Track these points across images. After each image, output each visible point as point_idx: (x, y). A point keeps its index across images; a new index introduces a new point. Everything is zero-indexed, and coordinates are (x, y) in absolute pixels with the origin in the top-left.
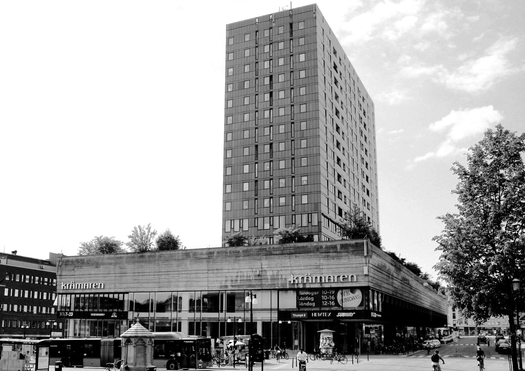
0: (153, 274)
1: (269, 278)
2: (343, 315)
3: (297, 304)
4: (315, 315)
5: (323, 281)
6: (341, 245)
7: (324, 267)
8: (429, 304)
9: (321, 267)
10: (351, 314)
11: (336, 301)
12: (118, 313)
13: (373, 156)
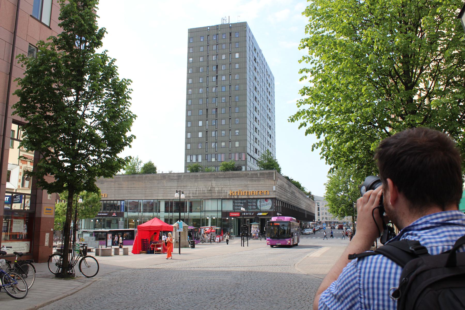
0: (141, 188)
1: (216, 192)
2: (261, 214)
3: (233, 208)
4: (244, 214)
5: (249, 194)
6: (260, 173)
7: (250, 186)
8: (305, 207)
9: (248, 186)
10: (265, 214)
11: (256, 206)
12: (117, 213)
13: (273, 112)
